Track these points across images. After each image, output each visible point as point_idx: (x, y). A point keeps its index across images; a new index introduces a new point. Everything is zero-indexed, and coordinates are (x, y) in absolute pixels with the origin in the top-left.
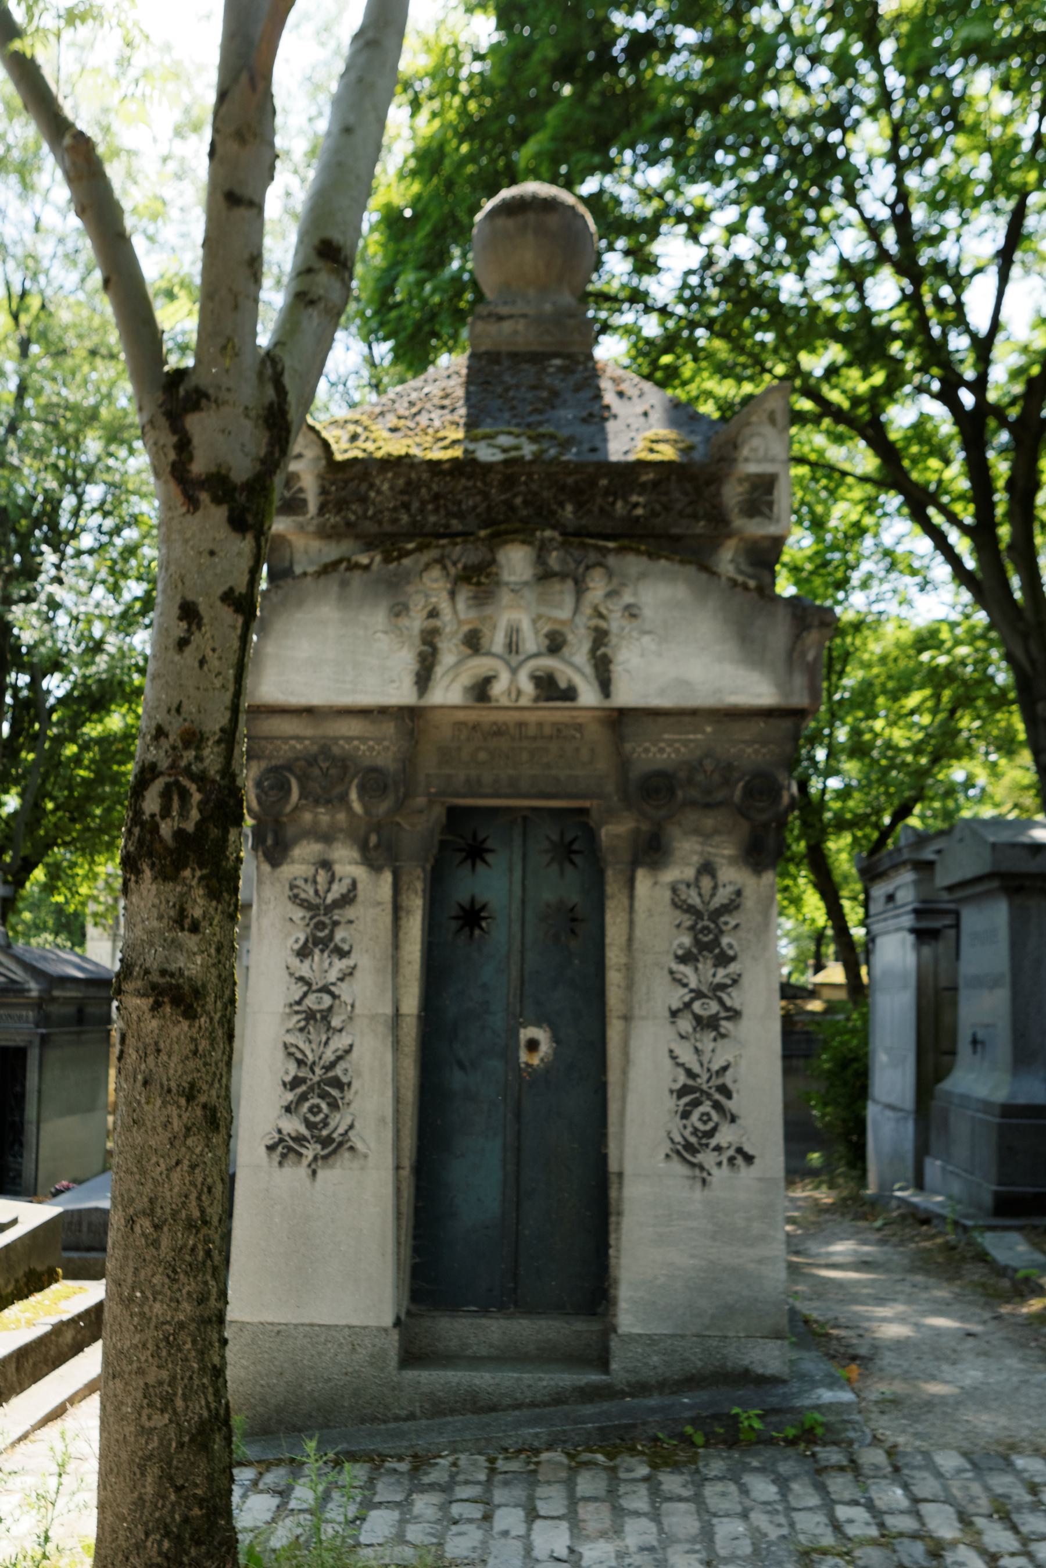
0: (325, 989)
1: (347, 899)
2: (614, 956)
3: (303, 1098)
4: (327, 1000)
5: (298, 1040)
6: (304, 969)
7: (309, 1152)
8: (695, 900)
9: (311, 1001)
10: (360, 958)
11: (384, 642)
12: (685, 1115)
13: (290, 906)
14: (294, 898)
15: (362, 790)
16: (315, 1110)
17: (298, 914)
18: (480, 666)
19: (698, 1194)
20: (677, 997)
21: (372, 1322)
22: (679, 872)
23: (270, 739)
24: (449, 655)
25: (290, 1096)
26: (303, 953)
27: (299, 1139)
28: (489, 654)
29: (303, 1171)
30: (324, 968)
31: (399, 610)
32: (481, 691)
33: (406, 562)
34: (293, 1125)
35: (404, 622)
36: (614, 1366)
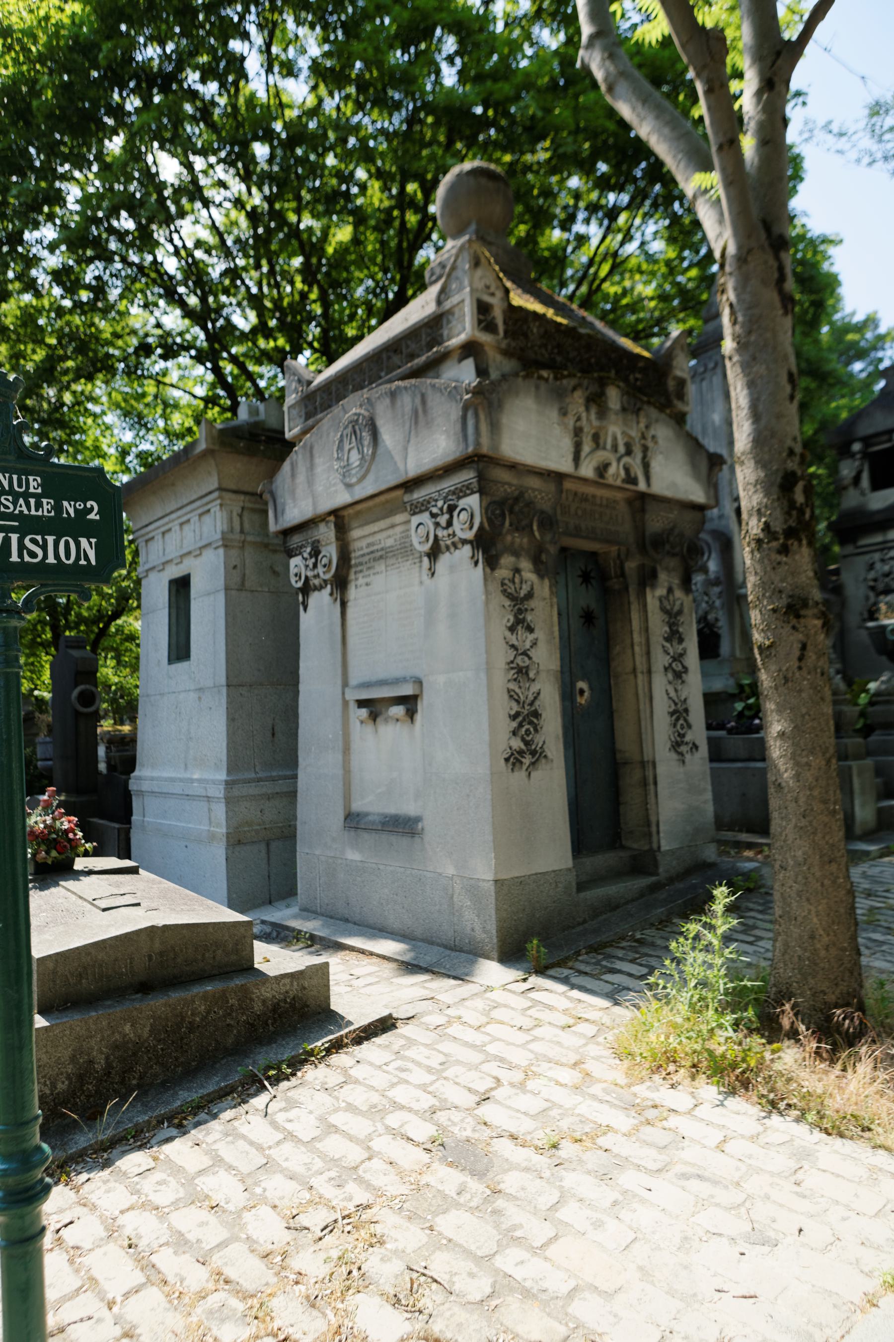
0: (525, 653)
1: (530, 595)
2: (556, 628)
3: (520, 725)
4: (527, 662)
5: (512, 686)
6: (513, 640)
7: (527, 761)
8: (511, 590)
9: (519, 660)
10: (539, 634)
11: (557, 430)
12: (675, 726)
13: (503, 598)
14: (504, 592)
15: (541, 525)
16: (528, 732)
17: (507, 603)
18: (602, 455)
19: (682, 770)
20: (667, 660)
21: (563, 867)
22: (661, 591)
23: (496, 482)
24: (586, 448)
25: (514, 724)
26: (512, 629)
27: (521, 753)
28: (604, 448)
29: (523, 774)
30: (524, 639)
31: (563, 412)
32: (602, 470)
33: (565, 382)
34: (517, 744)
35: (566, 420)
36: (661, 870)
